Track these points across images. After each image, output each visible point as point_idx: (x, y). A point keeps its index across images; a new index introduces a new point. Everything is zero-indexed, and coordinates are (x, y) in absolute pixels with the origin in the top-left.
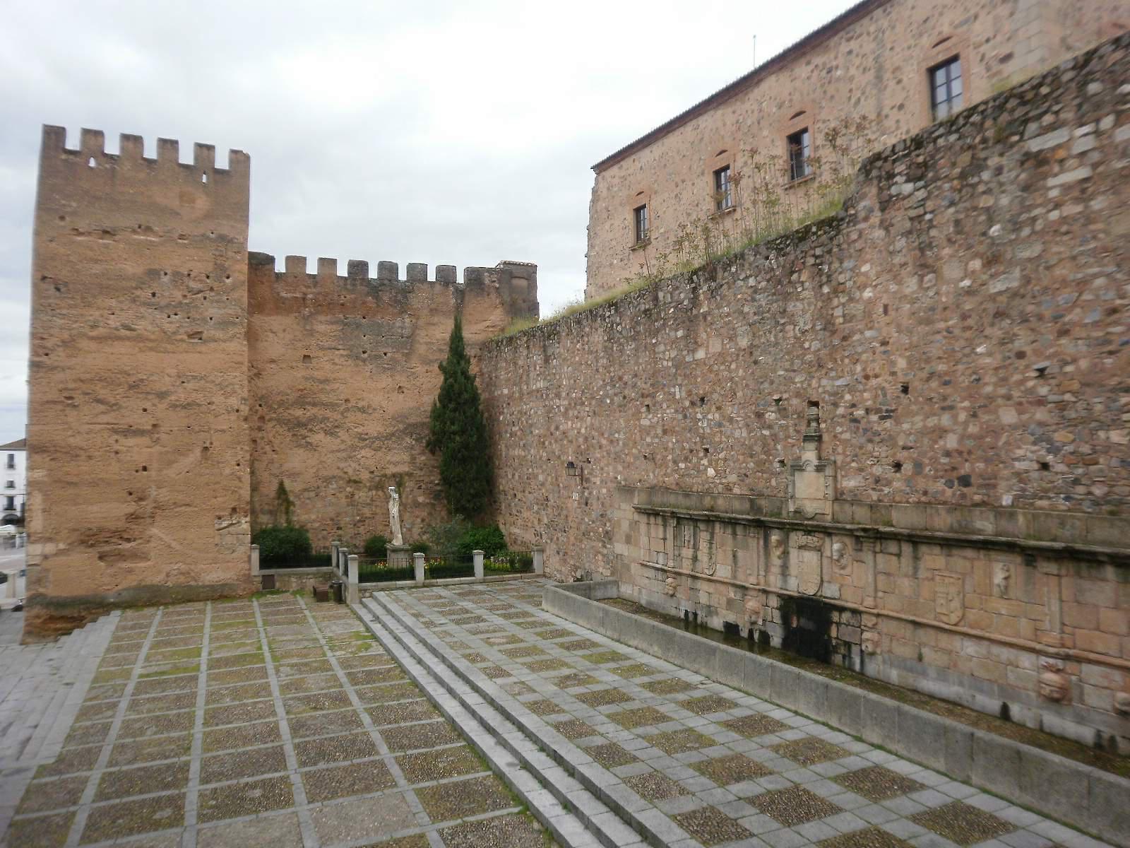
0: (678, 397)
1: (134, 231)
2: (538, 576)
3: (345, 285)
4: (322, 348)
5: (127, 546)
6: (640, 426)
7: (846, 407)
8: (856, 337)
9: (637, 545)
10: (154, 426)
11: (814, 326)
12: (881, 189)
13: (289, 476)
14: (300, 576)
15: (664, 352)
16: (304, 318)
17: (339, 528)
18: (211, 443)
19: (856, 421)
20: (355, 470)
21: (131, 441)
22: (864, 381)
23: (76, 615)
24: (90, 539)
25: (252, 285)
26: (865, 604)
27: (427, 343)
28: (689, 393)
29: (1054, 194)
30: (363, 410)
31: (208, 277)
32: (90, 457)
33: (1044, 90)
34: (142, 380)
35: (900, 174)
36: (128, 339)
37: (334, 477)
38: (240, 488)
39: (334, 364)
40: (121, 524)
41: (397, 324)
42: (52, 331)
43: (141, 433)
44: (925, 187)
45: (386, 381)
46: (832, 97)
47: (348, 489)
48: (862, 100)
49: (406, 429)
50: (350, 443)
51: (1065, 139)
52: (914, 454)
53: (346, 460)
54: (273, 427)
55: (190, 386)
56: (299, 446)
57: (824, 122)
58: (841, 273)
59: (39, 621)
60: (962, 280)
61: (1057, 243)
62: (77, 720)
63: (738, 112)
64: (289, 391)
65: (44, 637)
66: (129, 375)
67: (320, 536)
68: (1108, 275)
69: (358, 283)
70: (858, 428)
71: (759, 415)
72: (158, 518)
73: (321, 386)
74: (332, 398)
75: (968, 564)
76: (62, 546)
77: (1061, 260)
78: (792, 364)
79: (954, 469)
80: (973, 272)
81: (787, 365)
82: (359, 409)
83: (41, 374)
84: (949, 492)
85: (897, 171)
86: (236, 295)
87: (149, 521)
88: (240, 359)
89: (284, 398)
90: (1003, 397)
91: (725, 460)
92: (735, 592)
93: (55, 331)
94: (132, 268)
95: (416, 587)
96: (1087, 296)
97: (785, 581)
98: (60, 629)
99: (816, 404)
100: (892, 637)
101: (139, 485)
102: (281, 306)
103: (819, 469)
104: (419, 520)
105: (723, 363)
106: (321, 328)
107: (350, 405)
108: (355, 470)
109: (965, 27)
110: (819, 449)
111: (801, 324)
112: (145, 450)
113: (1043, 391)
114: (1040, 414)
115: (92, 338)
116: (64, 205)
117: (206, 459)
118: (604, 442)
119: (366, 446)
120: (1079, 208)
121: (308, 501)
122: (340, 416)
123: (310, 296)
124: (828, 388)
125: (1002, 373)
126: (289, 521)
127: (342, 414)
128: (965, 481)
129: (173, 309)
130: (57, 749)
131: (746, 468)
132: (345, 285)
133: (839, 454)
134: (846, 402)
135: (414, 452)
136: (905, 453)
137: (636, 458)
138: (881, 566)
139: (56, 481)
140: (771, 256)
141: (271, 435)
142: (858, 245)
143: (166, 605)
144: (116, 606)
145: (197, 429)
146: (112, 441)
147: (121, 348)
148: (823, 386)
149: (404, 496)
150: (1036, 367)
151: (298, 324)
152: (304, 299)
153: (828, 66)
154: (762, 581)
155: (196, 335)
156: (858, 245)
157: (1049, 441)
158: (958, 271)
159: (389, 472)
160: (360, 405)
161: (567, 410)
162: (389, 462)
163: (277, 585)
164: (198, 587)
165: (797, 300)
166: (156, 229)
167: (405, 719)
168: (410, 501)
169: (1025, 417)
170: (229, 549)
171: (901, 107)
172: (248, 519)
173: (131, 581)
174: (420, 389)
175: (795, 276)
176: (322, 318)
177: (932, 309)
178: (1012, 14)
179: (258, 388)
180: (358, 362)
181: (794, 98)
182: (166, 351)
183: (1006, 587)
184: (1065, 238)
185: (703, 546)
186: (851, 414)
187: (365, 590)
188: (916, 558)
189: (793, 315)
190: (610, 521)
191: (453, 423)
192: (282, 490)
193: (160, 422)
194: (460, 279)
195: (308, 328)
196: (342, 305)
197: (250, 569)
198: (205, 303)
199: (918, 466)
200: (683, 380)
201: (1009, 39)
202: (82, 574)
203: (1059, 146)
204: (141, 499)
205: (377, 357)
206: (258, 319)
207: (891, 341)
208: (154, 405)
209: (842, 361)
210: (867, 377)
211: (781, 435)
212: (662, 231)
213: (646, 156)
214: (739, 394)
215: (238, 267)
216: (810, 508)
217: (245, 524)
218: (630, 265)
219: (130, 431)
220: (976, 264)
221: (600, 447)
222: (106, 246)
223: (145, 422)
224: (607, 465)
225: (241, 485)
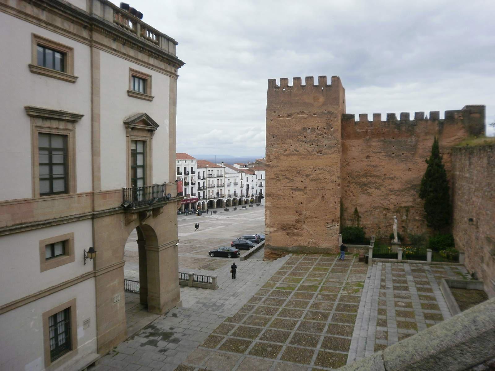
1: (298, 114)
2: (461, 265)
3: (385, 124)
5: (296, 231)
10: (305, 187)
13: (359, 206)
14: (358, 248)
16: (367, 140)
17: (379, 228)
18: (325, 194)
20: (388, 204)
21: (297, 193)
23: (279, 253)
24: (284, 227)
25: (343, 127)
27: (423, 148)
30: (392, 179)
31: (324, 129)
32: (284, 199)
34: (301, 170)
36: (296, 155)
37: (379, 207)
38: (336, 212)
39: (380, 159)
40: (294, 223)
41: (409, 141)
42: (272, 153)
45: (403, 166)
47: (384, 212)
49: (411, 187)
50: (386, 193)
54: (354, 186)
55: (318, 172)
56: (364, 193)
59: (268, 254)
62: (248, 302)
64: (360, 171)
65: (269, 259)
66: (296, 168)
67: (371, 231)
69: (391, 123)
72: (306, 222)
74: (379, 173)
76: (275, 229)
82: (390, 178)
83: (269, 169)
86: (335, 135)
87: (303, 222)
89: (359, 174)
93: (273, 153)
94: (298, 128)
95: (397, 262)
98: (274, 257)
101: (299, 209)
102: (357, 136)
104: (416, 227)
106: (374, 144)
107: (386, 176)
108: (388, 204)
112: (302, 196)
115: (285, 155)
116: (275, 107)
117: (324, 200)
119: (393, 194)
121: (366, 216)
122: (382, 181)
123: (369, 131)
126: (358, 224)
127: (383, 180)
129: (311, 142)
130: (236, 312)
132: (385, 124)
135: (415, 197)
141: (352, 189)
143: (307, 254)
144: (291, 252)
145: (320, 189)
147: (294, 158)
149: (409, 216)
151: (364, 142)
152: (367, 132)
155: (320, 152)
159: (403, 205)
160: (391, 176)
162: (403, 201)
163: (349, 251)
164: (319, 248)
166: (305, 112)
167: (338, 334)
168: (412, 218)
170: (331, 235)
173: (296, 244)
174: (417, 170)
176: (375, 140)
179: (348, 169)
180: (390, 158)
182: (309, 159)
187: (375, 261)
191: (430, 187)
192: (356, 211)
195: (368, 144)
196: (384, 133)
197: (338, 244)
198: (323, 139)
204: (300, 214)
205: (399, 156)
206: (348, 142)
208: (305, 180)
215: (335, 124)
217: (337, 226)
219: (297, 189)
222: (289, 121)
223: (301, 186)
225: (336, 211)
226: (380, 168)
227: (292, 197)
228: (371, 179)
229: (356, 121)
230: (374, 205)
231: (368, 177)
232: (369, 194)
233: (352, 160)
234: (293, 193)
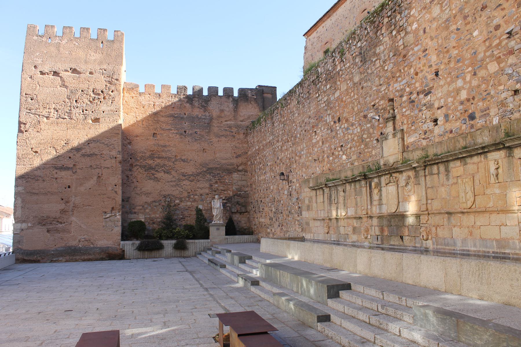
10: (74, 165)
18: (102, 174)
19: (413, 101)
21: (63, 173)
27: (218, 127)
28: (333, 117)
30: (184, 161)
40: (58, 215)
43: (68, 169)
49: (207, 170)
50: (177, 178)
52: (444, 110)
53: (175, 186)
54: (137, 169)
64: (146, 151)
71: (365, 117)
73: (162, 149)
74: (169, 155)
75: (475, 167)
76: (30, 225)
79: (466, 111)
84: (464, 127)
87: (71, 213)
88: (118, 132)
89: (143, 155)
91: (351, 148)
92: (357, 222)
97: (380, 209)
100: (437, 227)
111: (383, 58)
121: (155, 208)
122: (172, 164)
124: (398, 88)
125: (487, 44)
127: (173, 163)
131: (360, 149)
133: (405, 124)
134: (407, 93)
135: (211, 182)
139: (27, 192)
141: (136, 173)
145: (95, 167)
146: (54, 172)
150: (507, 31)
160: (183, 158)
162: (198, 188)
164: (94, 248)
172: (120, 213)
185: (341, 199)
188: (447, 171)
193: (77, 164)
194: (236, 94)
199: (446, 116)
202: (41, 240)
208: (74, 155)
209: (404, 69)
213: (328, 23)
226: (170, 148)
227: (56, 179)
228: (158, 161)
231: (155, 159)
232: (157, 180)
233: (135, 138)
234: (56, 173)
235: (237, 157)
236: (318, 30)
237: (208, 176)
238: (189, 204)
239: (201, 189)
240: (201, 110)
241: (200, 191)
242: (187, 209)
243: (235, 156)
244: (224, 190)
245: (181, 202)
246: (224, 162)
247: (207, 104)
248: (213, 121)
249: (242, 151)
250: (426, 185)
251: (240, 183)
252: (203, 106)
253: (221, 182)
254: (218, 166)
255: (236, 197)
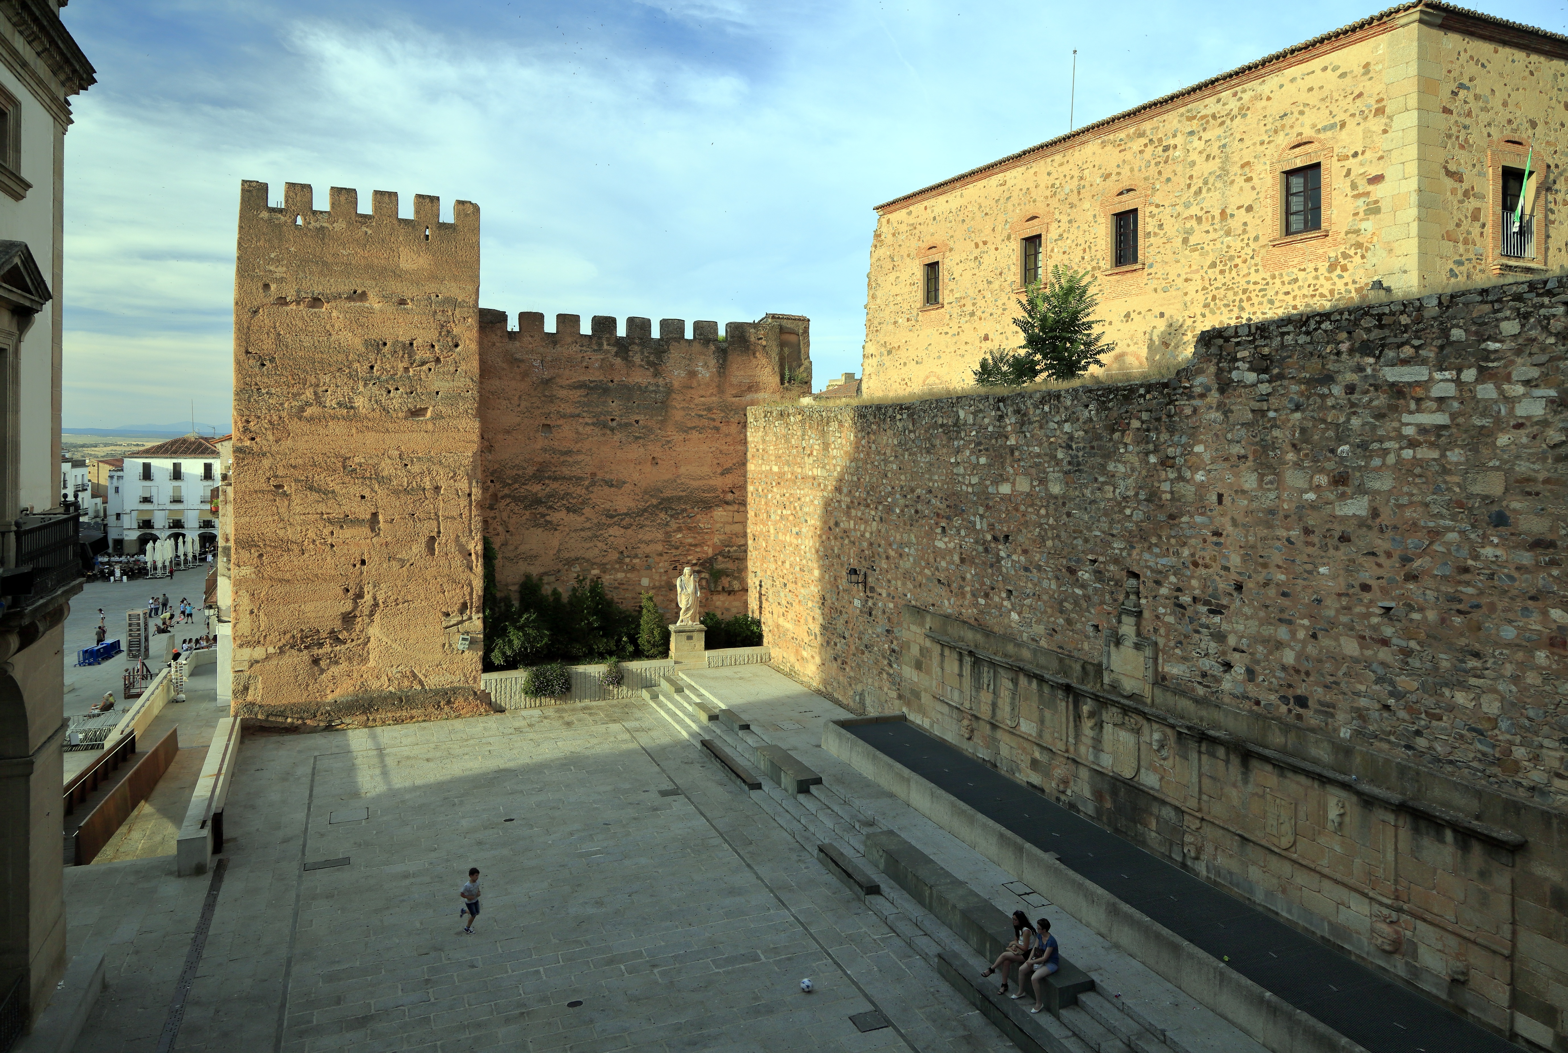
0: (978, 527)
4: (564, 416)
6: (935, 547)
7: (1170, 589)
8: (1185, 519)
9: (928, 672)
11: (1137, 494)
12: (1220, 370)
15: (964, 476)
19: (1181, 606)
21: (348, 533)
22: (1191, 567)
26: (1188, 804)
28: (991, 527)
29: (1409, 431)
33: (1404, 320)
35: (1243, 359)
44: (1269, 382)
46: (1169, 180)
48: (1204, 190)
49: (660, 503)
50: (596, 521)
51: (1426, 378)
53: (591, 539)
54: (507, 505)
57: (1157, 206)
58: (1170, 446)
60: (1306, 491)
61: (1409, 483)
63: (1054, 175)
64: (525, 465)
68: (1462, 532)
70: (1183, 615)
71: (1072, 571)
74: (576, 471)
77: (1411, 503)
78: (1111, 528)
79: (1290, 686)
80: (1319, 486)
81: (1105, 526)
82: (606, 482)
84: (1284, 709)
85: (1239, 355)
89: (520, 472)
90: (1345, 625)
96: (1437, 547)
99: (1136, 576)
103: (1137, 647)
105: (1032, 505)
109: (1329, 134)
110: (1138, 625)
113: (1388, 631)
114: (1384, 654)
118: (892, 553)
120: (1435, 454)
122: (584, 491)
127: (587, 488)
128: (1302, 701)
134: (1171, 583)
135: (668, 529)
136: (1237, 655)
137: (928, 579)
138: (1205, 769)
140: (1091, 407)
142: (1191, 422)
146: (326, 532)
148: (1146, 560)
153: (1164, 144)
154: (1072, 749)
156: (1191, 422)
157: (1392, 683)
158: (1300, 484)
160: (607, 477)
161: (848, 507)
162: (641, 541)
165: (1119, 462)
169: (1368, 653)
171: (1249, 209)
175: (1117, 435)
177: (1272, 512)
178: (1385, 131)
181: (1123, 171)
183: (1340, 824)
184: (1417, 480)
185: (1005, 694)
186: (1177, 598)
189: (1113, 476)
190: (897, 639)
200: (985, 512)
201: (1381, 158)
203: (1418, 383)
205: (627, 425)
207: (1224, 533)
210: (1196, 564)
211: (1096, 599)
212: (958, 295)
213: (940, 204)
214: (1049, 543)
216: (1129, 685)
218: (917, 327)
219: (346, 521)
220: (1322, 479)
221: (887, 558)
224: (896, 579)
226: (579, 458)
228: (555, 485)
229: (509, 329)
230: (566, 555)
234: (332, 533)
235: (722, 474)
236: (911, 208)
237: (662, 515)
238: (620, 575)
239: (647, 543)
240: (648, 373)
241: (645, 549)
242: (616, 588)
243: (719, 471)
244: (696, 545)
245: (604, 572)
246: (695, 484)
247: (660, 358)
248: (674, 396)
249: (735, 461)
250: (1200, 768)
251: (728, 529)
252: (651, 364)
253: (689, 529)
254: (684, 494)
255: (720, 558)
